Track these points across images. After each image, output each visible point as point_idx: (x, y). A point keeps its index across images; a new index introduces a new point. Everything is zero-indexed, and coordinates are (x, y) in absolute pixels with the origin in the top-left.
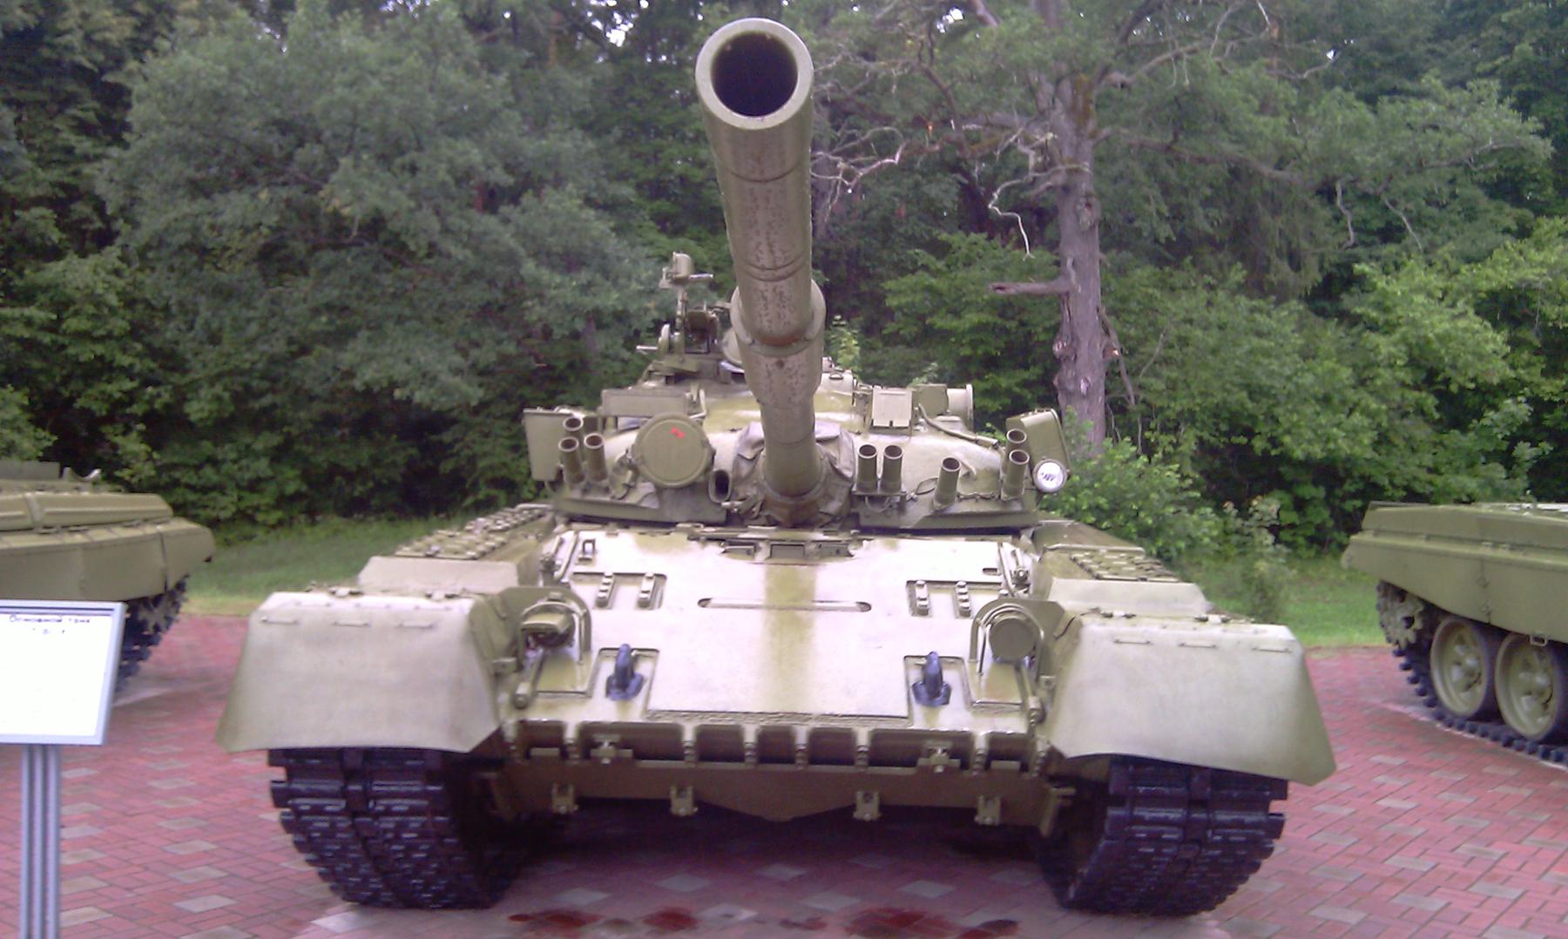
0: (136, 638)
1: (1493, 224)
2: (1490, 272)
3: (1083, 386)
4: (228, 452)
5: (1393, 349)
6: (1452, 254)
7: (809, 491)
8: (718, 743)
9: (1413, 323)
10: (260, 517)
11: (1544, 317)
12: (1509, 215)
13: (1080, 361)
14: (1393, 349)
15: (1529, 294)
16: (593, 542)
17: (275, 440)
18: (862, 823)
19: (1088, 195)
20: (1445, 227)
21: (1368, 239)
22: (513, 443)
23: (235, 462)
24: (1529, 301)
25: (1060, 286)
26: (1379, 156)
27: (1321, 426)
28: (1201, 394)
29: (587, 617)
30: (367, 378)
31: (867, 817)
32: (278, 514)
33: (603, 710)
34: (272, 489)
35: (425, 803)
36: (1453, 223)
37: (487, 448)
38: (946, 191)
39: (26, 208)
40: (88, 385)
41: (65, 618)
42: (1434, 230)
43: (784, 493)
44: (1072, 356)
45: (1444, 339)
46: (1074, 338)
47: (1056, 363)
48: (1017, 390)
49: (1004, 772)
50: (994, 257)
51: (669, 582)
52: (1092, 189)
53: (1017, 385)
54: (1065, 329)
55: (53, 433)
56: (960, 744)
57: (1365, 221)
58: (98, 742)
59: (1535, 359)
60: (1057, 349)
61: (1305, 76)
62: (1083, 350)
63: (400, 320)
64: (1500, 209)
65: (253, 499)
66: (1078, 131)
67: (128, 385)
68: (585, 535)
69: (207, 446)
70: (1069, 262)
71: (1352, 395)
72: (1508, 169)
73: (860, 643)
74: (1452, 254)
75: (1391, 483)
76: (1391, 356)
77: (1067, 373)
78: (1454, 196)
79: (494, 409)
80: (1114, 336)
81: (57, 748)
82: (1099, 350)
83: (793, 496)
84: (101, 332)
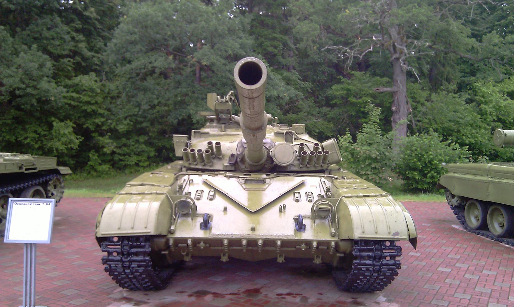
2: (509, 87)
4: (131, 142)
8: (235, 242)
10: (141, 164)
13: (400, 113)
17: (146, 138)
18: (279, 263)
21: (466, 75)
23: (133, 145)
25: (394, 89)
27: (473, 133)
28: (441, 123)
29: (194, 203)
31: (281, 261)
32: (147, 163)
33: (200, 234)
34: (146, 155)
39: (63, 59)
40: (87, 120)
41: (32, 203)
42: (485, 73)
44: (398, 112)
46: (399, 105)
49: (323, 249)
54: (396, 102)
55: (82, 136)
56: (308, 243)
57: (464, 70)
61: (472, 10)
65: (140, 158)
67: (103, 120)
69: (124, 140)
70: (399, 82)
71: (481, 124)
73: (281, 212)
80: (410, 105)
81: (35, 244)
82: (406, 109)
84: (93, 102)
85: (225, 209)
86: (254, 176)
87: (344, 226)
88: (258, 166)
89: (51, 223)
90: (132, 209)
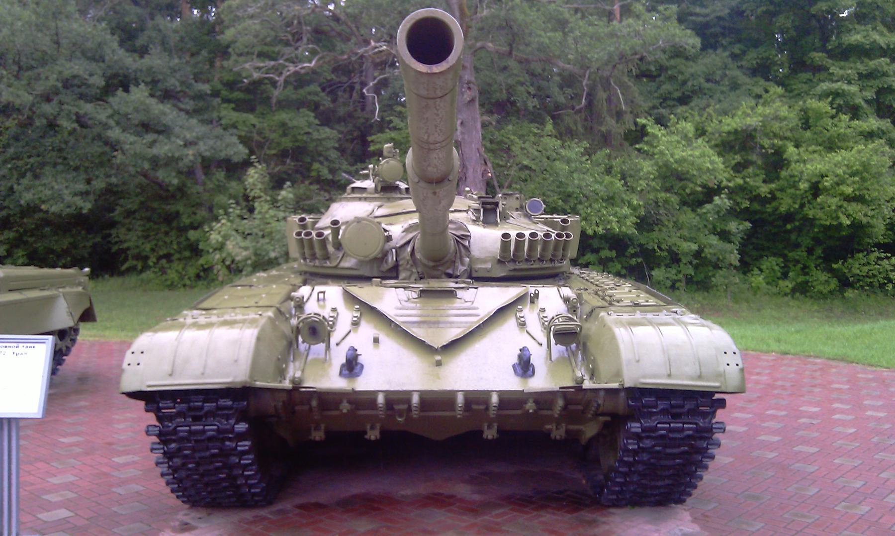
0: (58, 356)
7: (443, 258)
8: (397, 401)
9: (661, 153)
11: (762, 147)
13: (468, 180)
14: (650, 169)
15: (753, 133)
16: (324, 293)
19: (469, 82)
20: (718, 95)
22: (145, 234)
27: (604, 215)
30: (28, 198)
35: (659, 473)
36: (722, 92)
37: (128, 237)
41: (21, 345)
43: (429, 259)
45: (680, 161)
50: (575, 123)
57: (670, 93)
58: (40, 416)
59: (758, 172)
62: (470, 173)
63: (55, 165)
68: (318, 288)
72: (762, 58)
73: (498, 350)
74: (715, 110)
75: (659, 247)
76: (649, 173)
79: (137, 215)
80: (489, 165)
81: (17, 420)
82: (479, 173)
83: (435, 261)
85: (376, 341)
86: (435, 284)
87: (604, 368)
88: (437, 265)
89: (45, 382)
90: (203, 344)
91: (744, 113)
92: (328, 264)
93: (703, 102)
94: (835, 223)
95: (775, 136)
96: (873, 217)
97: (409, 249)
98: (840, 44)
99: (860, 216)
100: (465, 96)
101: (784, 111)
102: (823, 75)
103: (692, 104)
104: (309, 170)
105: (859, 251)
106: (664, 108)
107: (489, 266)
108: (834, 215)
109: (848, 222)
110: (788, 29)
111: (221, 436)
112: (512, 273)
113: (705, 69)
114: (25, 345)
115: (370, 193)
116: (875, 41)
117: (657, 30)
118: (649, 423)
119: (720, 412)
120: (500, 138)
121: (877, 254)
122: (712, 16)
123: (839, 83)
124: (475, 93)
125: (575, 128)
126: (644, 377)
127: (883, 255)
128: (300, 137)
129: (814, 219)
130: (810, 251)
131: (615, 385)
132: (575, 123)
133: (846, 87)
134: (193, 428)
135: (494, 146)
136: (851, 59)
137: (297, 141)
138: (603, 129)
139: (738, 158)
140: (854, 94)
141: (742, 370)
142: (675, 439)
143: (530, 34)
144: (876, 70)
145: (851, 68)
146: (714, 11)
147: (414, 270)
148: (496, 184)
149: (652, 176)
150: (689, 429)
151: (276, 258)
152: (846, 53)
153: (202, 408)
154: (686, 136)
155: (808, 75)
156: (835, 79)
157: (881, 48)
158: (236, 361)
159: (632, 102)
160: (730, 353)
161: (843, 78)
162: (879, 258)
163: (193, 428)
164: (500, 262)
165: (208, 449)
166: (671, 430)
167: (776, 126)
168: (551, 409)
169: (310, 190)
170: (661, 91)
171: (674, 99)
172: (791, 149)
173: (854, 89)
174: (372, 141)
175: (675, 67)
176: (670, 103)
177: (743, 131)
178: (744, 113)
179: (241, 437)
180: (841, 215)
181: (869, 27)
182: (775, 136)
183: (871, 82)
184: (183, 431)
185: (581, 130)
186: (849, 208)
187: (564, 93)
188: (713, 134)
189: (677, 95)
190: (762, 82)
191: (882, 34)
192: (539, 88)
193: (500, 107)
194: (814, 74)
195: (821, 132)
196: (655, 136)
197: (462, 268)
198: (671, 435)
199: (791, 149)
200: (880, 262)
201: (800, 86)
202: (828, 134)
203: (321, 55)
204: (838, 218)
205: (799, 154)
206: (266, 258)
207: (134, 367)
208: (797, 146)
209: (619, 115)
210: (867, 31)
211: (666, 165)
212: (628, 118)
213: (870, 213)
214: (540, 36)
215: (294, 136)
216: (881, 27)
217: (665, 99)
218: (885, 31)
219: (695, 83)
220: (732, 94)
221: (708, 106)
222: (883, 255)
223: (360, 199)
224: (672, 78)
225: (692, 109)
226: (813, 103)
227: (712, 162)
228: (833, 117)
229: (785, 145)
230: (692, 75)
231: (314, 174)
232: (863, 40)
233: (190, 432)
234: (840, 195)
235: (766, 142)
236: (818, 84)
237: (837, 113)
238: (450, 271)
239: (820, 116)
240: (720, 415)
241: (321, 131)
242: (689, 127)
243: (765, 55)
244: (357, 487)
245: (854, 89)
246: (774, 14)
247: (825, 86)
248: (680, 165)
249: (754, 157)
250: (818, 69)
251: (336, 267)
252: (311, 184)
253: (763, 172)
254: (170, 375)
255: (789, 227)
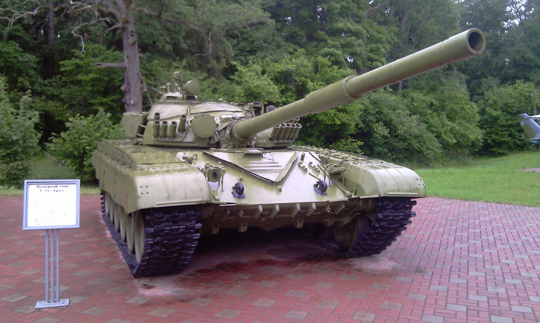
1: (286, 50)
3: (132, 102)
5: (240, 90)
6: (270, 59)
9: (247, 82)
11: (296, 81)
12: (291, 47)
14: (240, 90)
19: (132, 32)
20: (270, 51)
24: (291, 76)
26: (220, 22)
36: (272, 49)
38: (98, 29)
42: (267, 51)
45: (257, 87)
46: (129, 84)
47: (123, 94)
48: (110, 103)
50: (193, 61)
51: (278, 194)
52: (134, 30)
53: (110, 101)
54: (126, 81)
57: (244, 48)
58: (78, 226)
59: (293, 95)
60: (123, 88)
64: (289, 45)
66: (127, 8)
72: (292, 32)
74: (270, 59)
76: (240, 93)
77: (127, 97)
78: (273, 40)
80: (145, 84)
82: (139, 89)
91: (286, 62)
92: (176, 140)
93: (262, 55)
94: (332, 123)
95: (302, 75)
96: (350, 120)
97: (228, 132)
98: (332, 28)
99: (345, 120)
100: (130, 40)
101: (306, 62)
102: (323, 44)
103: (257, 55)
104: (17, 82)
105: (342, 138)
106: (241, 55)
107: (265, 141)
108: (332, 119)
109: (340, 123)
110: (306, 17)
111: (187, 231)
112: (276, 145)
113: (264, 36)
114: (62, 185)
115: (180, 100)
116: (349, 28)
117: (252, 11)
118: (385, 213)
119: (414, 207)
120: (150, 68)
121: (351, 140)
122: (267, 6)
123: (333, 49)
124: (135, 38)
125: (192, 64)
126: (389, 192)
127: (353, 140)
128: (10, 60)
129: (322, 121)
130: (318, 138)
131: (377, 196)
132: (193, 61)
133: (336, 51)
134: (173, 227)
135: (147, 73)
136: (337, 36)
137: (7, 62)
138: (210, 66)
139: (283, 87)
140: (340, 55)
141: (425, 187)
142: (395, 220)
143: (176, 6)
144: (349, 43)
145: (337, 41)
146: (268, 3)
147: (231, 143)
148: (149, 96)
149: (242, 95)
150: (402, 215)
151: (17, 140)
152: (335, 33)
153: (178, 216)
154: (257, 72)
155: (316, 43)
156: (330, 46)
157: (352, 30)
158: (201, 190)
159: (225, 51)
160: (419, 180)
161: (333, 45)
162: (353, 142)
163: (173, 227)
164: (271, 139)
165: (177, 239)
166: (394, 216)
167: (302, 70)
168: (290, 214)
169: (18, 95)
170: (239, 46)
171: (246, 51)
172: (310, 83)
173: (340, 52)
174: (63, 65)
175: (247, 33)
176: (244, 53)
177: (286, 72)
178: (286, 62)
179: (197, 231)
180: (336, 119)
181: (346, 19)
182: (302, 75)
183: (347, 49)
184: (167, 230)
185: (196, 66)
186: (340, 116)
187: (186, 43)
188: (270, 72)
189: (248, 49)
190: (292, 45)
191: (352, 24)
192: (172, 38)
193: (143, 48)
194: (318, 43)
195: (324, 75)
196: (242, 72)
197: (253, 143)
198: (395, 219)
199: (310, 83)
200: (352, 144)
201: (312, 49)
202: (328, 76)
203: (40, 7)
204: (334, 120)
205: (313, 86)
206: (10, 140)
207: (145, 195)
208: (312, 81)
209: (218, 58)
210: (345, 21)
211: (249, 88)
212: (223, 60)
213: (349, 118)
214: (181, 8)
215: (6, 59)
216: (351, 20)
217: (242, 51)
218: (353, 22)
219: (259, 43)
220: (277, 51)
221: (266, 56)
222: (353, 140)
223: (175, 103)
224: (245, 39)
225: (257, 57)
226: (320, 59)
227: (273, 88)
228: (329, 67)
229: (306, 81)
230: (257, 39)
231: (19, 84)
232: (343, 26)
233: (171, 230)
234: (336, 108)
235: (298, 79)
236: (321, 49)
237: (332, 65)
238: (249, 144)
239: (323, 65)
240: (414, 208)
241: (25, 56)
242: (259, 69)
243: (294, 30)
244: (228, 259)
245: (340, 52)
246: (299, 8)
247: (326, 50)
248: (257, 90)
249: (291, 87)
250: (321, 40)
251: (181, 142)
252: (18, 91)
253: (296, 95)
254: (168, 198)
255: (308, 125)
